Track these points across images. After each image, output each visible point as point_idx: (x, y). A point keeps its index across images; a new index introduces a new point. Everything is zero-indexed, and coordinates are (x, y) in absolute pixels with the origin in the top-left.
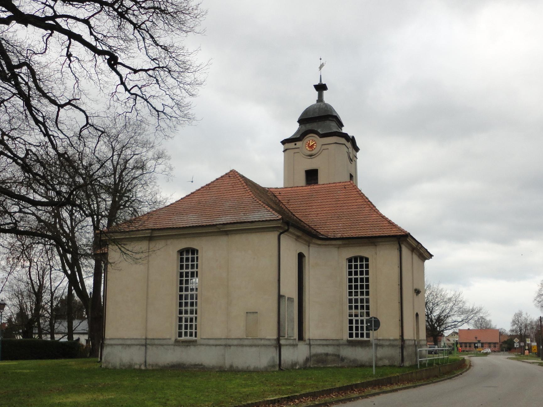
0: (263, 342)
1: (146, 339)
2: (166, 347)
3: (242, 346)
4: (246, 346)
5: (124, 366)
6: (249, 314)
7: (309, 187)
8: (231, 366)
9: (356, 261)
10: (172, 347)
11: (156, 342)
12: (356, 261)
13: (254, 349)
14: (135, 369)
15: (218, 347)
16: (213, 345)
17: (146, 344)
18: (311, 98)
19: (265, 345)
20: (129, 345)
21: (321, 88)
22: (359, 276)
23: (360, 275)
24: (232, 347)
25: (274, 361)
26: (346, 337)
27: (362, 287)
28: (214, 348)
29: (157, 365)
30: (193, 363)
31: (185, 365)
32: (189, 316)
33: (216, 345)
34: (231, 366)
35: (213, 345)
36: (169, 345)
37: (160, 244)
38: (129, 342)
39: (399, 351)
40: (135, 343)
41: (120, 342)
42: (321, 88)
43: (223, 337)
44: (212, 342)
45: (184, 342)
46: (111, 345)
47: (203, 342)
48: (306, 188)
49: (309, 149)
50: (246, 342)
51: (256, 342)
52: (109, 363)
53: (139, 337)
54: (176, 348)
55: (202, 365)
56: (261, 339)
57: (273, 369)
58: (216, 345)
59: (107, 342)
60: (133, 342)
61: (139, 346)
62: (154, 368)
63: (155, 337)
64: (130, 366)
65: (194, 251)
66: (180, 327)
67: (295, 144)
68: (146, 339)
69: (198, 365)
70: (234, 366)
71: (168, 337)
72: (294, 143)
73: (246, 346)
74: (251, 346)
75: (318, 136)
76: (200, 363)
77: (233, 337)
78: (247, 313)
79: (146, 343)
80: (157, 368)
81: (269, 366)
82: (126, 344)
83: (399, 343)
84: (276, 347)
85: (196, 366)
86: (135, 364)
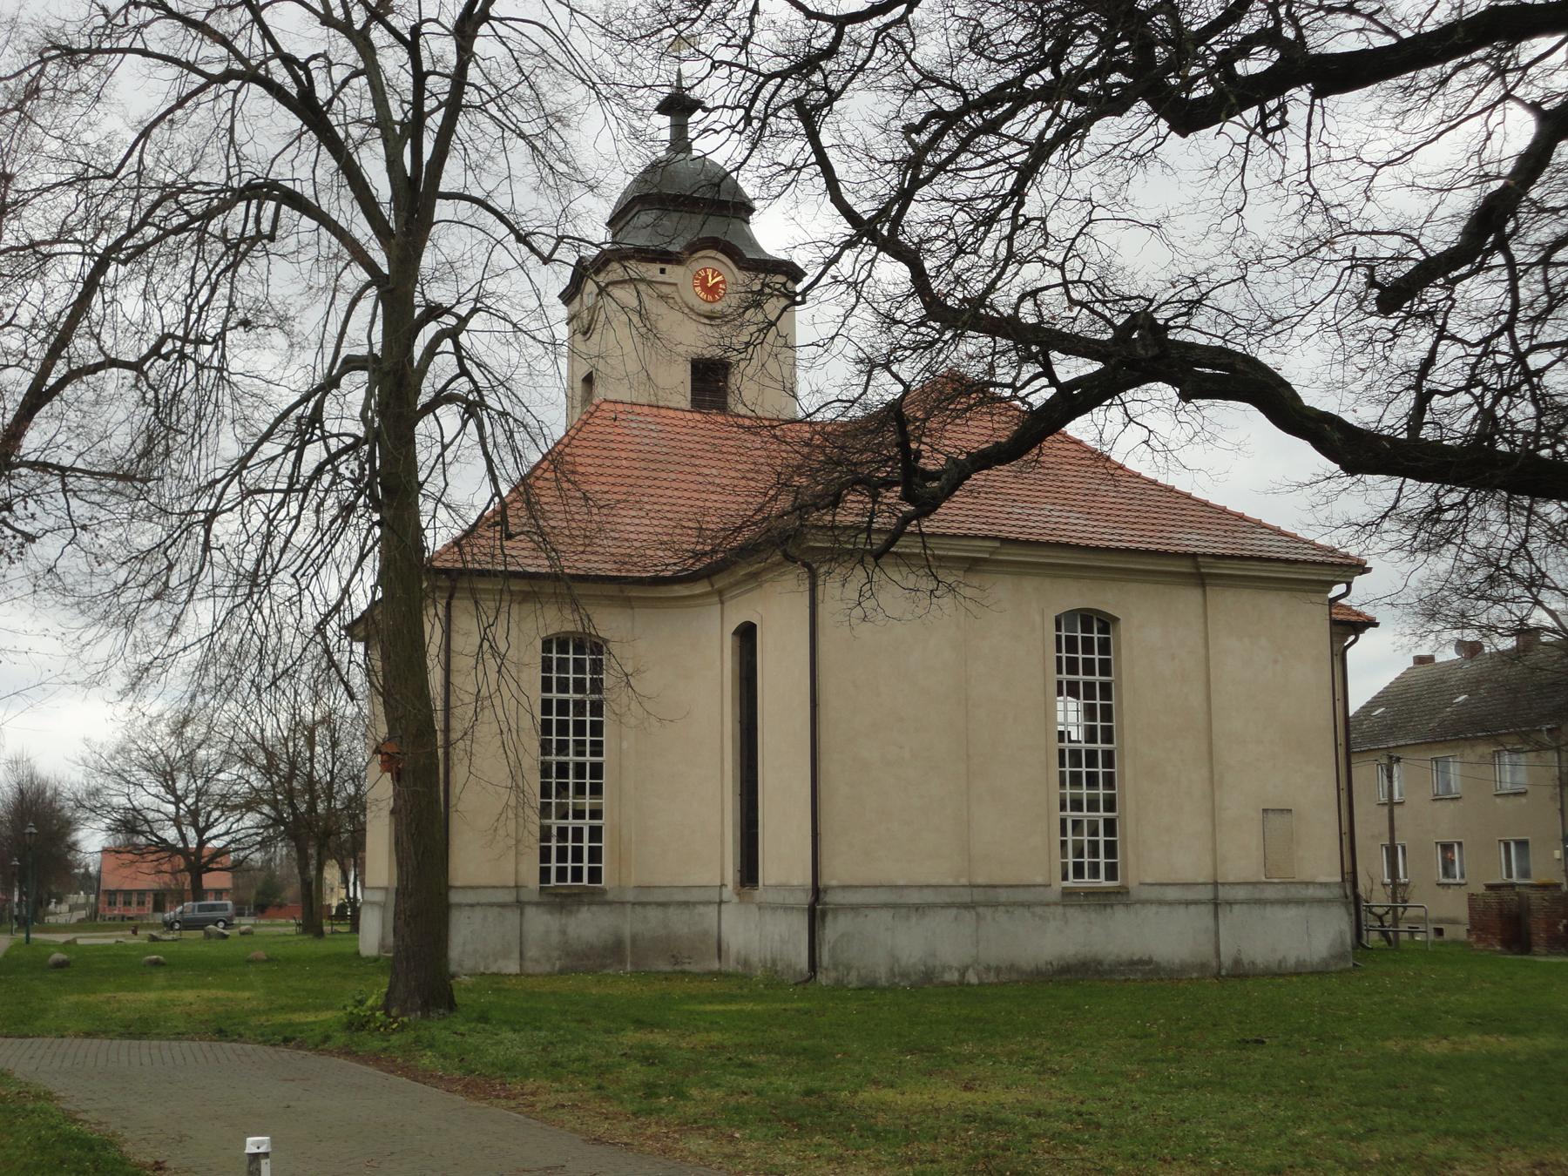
0: (1311, 892)
1: (1216, 884)
2: (1039, 910)
3: (1262, 902)
4: (1273, 902)
5: (905, 975)
6: (1271, 815)
7: (697, 416)
8: (1237, 962)
9: (563, 648)
10: (1060, 910)
11: (1003, 895)
12: (563, 648)
13: (1292, 912)
14: (947, 985)
15: (1192, 908)
16: (1180, 903)
17: (977, 900)
19: (1320, 901)
20: (917, 908)
22: (571, 696)
23: (559, 691)
24: (1236, 908)
25: (1343, 943)
26: (532, 880)
27: (580, 728)
28: (1181, 910)
29: (1012, 968)
30: (1125, 957)
31: (1100, 963)
32: (571, 823)
33: (1187, 903)
34: (1237, 962)
35: (1180, 903)
36: (1048, 905)
37: (1001, 590)
38: (914, 897)
39: (801, 924)
40: (939, 900)
41: (883, 897)
43: (1201, 880)
44: (1172, 894)
45: (1091, 893)
46: (855, 908)
47: (1147, 893)
48: (689, 416)
49: (703, 295)
50: (1270, 893)
51: (1294, 892)
52: (849, 968)
53: (950, 881)
54: (1071, 912)
55: (1150, 961)
56: (1307, 884)
57: (1342, 965)
58: (1187, 903)
59: (454, 897)
60: (929, 897)
61: (954, 911)
62: (1004, 977)
63: (996, 881)
64: (928, 976)
65: (1107, 623)
66: (1111, 849)
67: (663, 271)
68: (1216, 884)
69: (1141, 962)
70: (1246, 960)
71: (1039, 880)
72: (657, 267)
73: (1170, 903)
74: (1286, 902)
75: (735, 262)
76: (1146, 958)
77: (1231, 879)
78: (1265, 811)
79: (1216, 898)
80: (1014, 976)
81: (1333, 957)
82: (907, 904)
83: (805, 899)
84: (1346, 905)
85: (1133, 964)
86: (946, 968)
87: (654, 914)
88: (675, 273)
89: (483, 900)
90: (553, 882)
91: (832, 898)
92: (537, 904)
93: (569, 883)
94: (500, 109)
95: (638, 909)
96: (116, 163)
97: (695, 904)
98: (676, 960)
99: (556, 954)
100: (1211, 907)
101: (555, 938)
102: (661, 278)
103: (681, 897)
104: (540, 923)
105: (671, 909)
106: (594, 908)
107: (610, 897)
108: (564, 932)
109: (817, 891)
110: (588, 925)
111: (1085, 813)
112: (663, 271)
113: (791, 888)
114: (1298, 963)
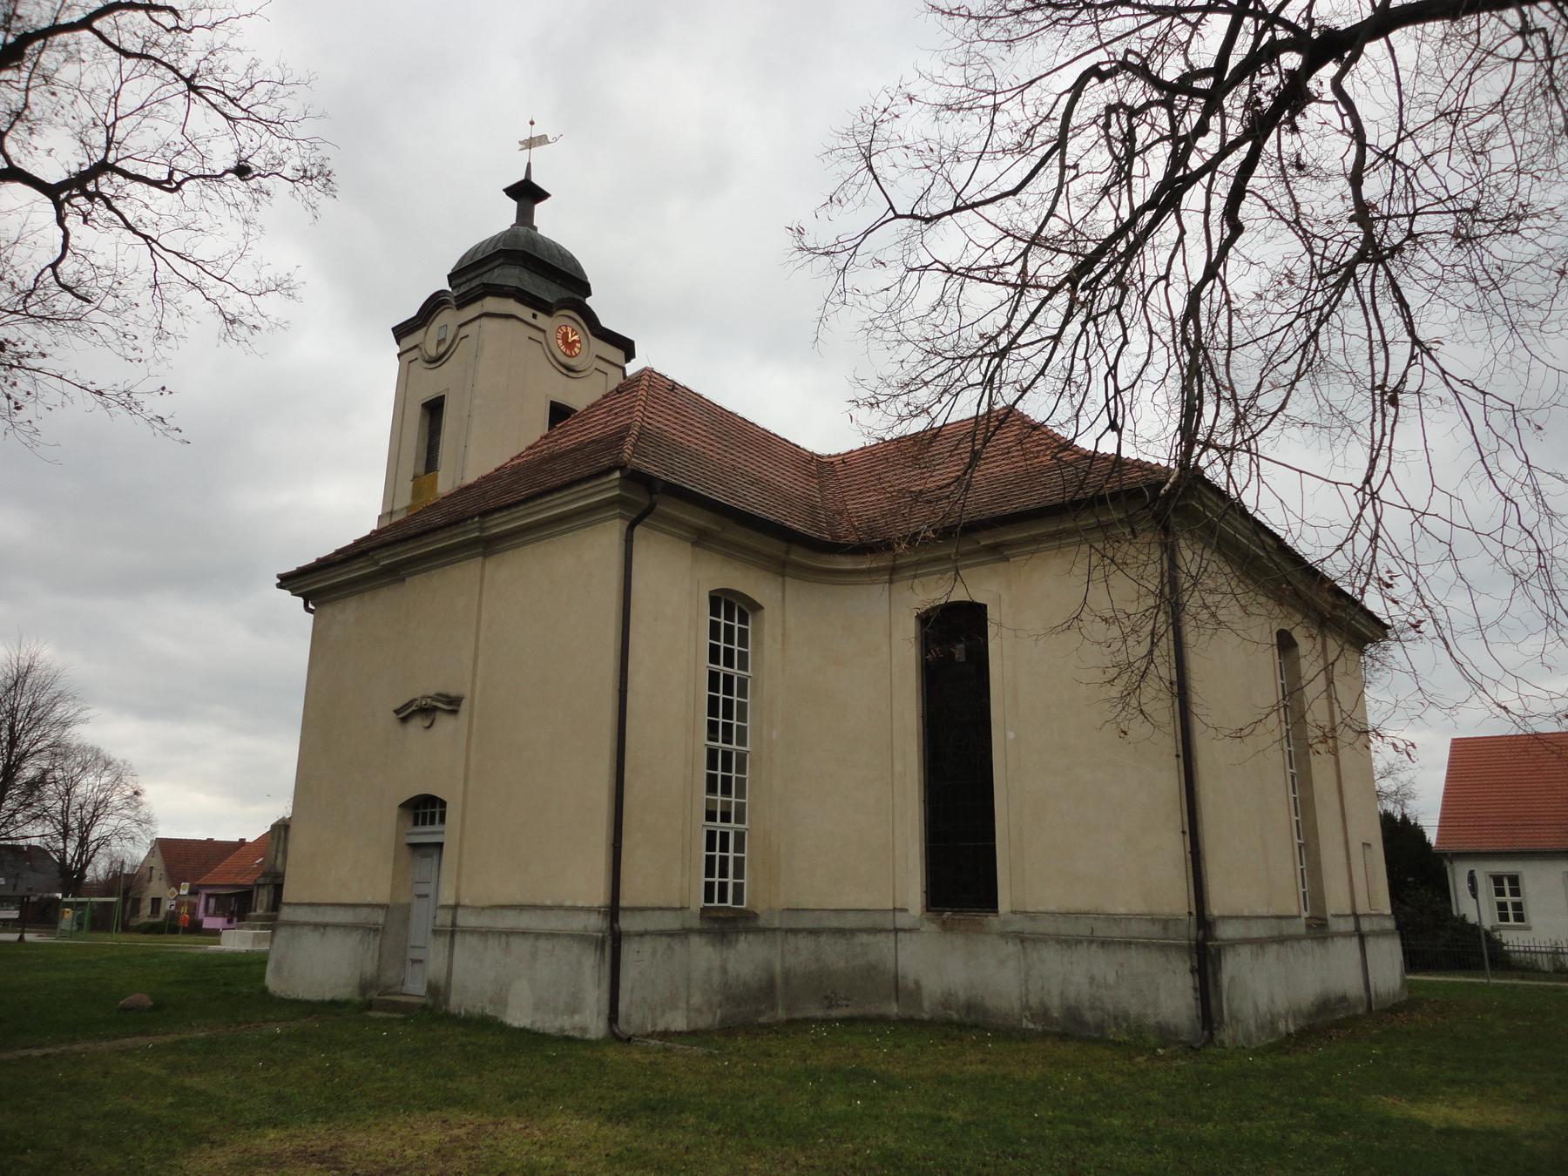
1: (456, 907)
18: (505, 215)
21: (526, 193)
42: (526, 193)
83: (1187, 932)
87: (805, 944)
88: (542, 321)
89: (651, 927)
90: (730, 903)
91: (1225, 931)
92: (700, 932)
93: (716, 904)
94: (1335, 272)
95: (791, 938)
96: (1402, 281)
97: (853, 931)
98: (830, 1002)
99: (717, 999)
100: (1355, 941)
101: (716, 978)
102: (532, 321)
103: (834, 922)
104: (703, 954)
105: (823, 939)
106: (751, 937)
107: (761, 923)
108: (724, 971)
109: (613, 910)
110: (747, 958)
111: (733, 824)
112: (534, 316)
113: (1166, 923)
114: (946, 1003)
